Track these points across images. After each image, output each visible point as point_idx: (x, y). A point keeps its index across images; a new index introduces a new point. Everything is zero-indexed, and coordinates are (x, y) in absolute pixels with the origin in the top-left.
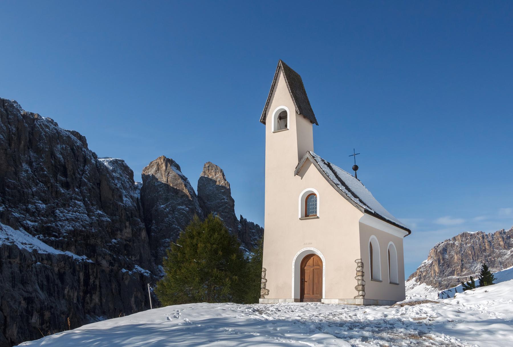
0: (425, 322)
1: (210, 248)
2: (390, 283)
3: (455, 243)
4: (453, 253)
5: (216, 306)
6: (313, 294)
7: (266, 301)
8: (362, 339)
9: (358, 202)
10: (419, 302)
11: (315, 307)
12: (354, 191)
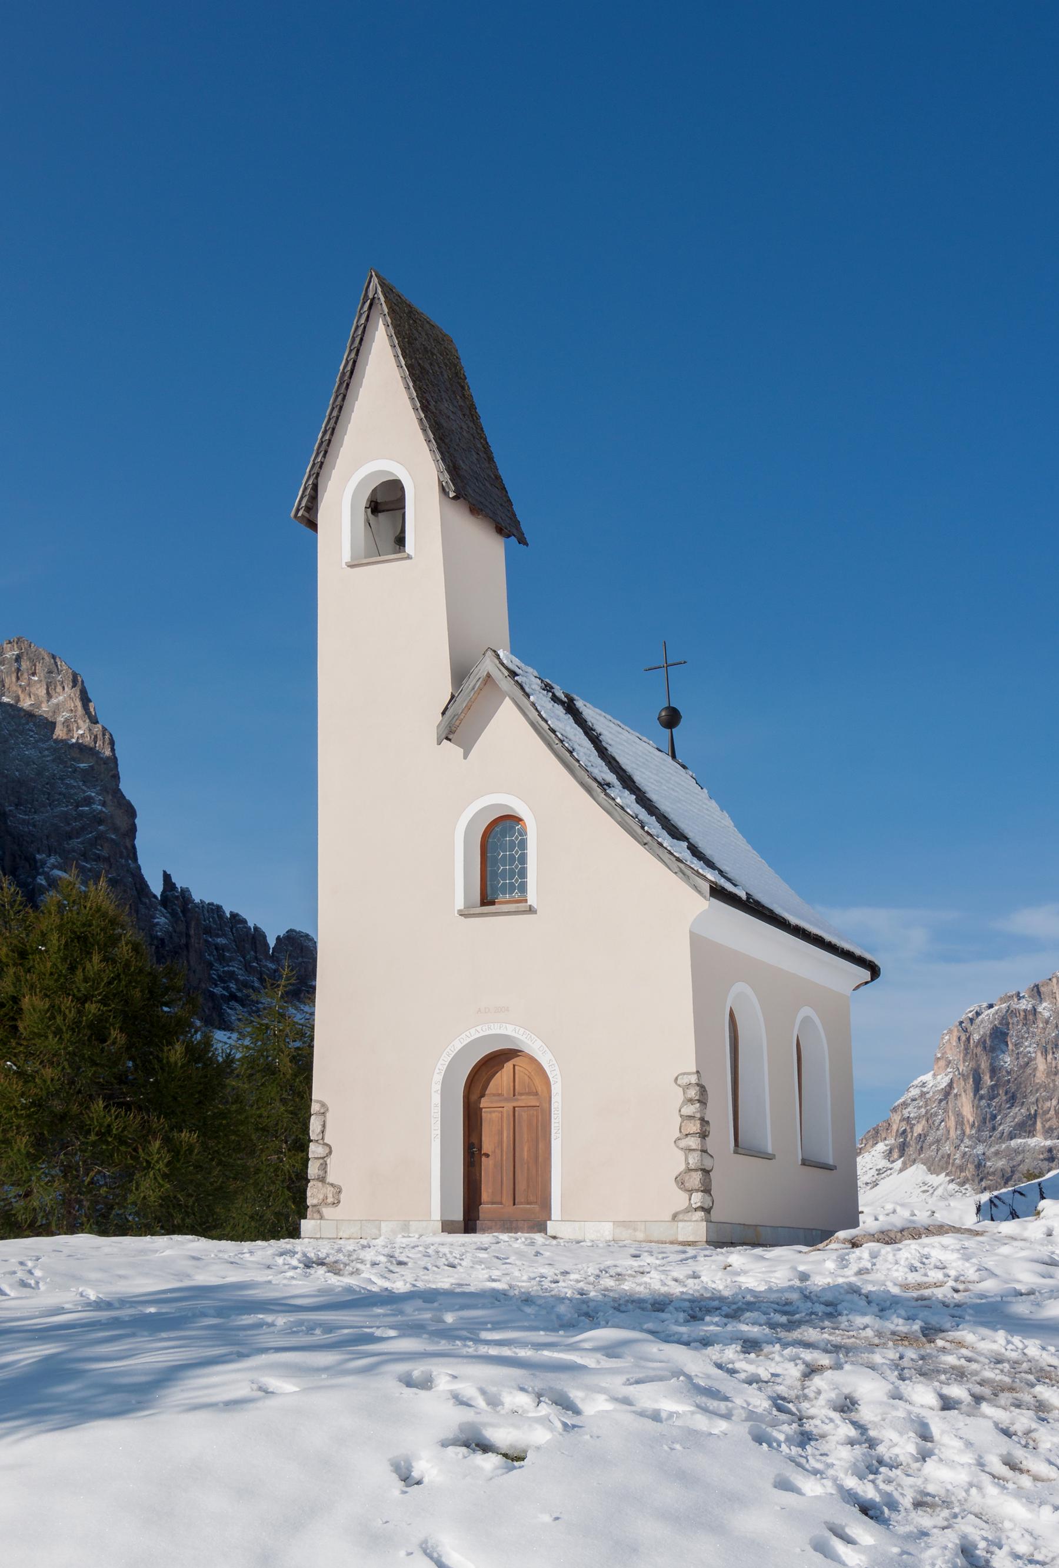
0: (940, 1296)
1: (72, 1015)
2: (804, 1162)
3: (1040, 1009)
4: (1029, 1047)
5: (156, 1240)
6: (514, 1204)
7: (327, 1229)
8: (742, 1347)
9: (687, 855)
10: (914, 1232)
11: (531, 1251)
12: (669, 810)
